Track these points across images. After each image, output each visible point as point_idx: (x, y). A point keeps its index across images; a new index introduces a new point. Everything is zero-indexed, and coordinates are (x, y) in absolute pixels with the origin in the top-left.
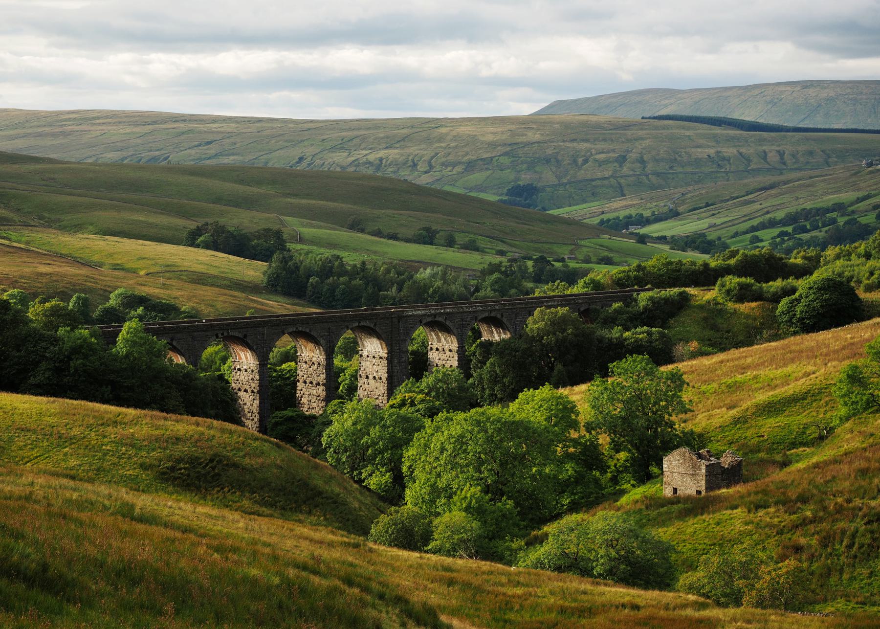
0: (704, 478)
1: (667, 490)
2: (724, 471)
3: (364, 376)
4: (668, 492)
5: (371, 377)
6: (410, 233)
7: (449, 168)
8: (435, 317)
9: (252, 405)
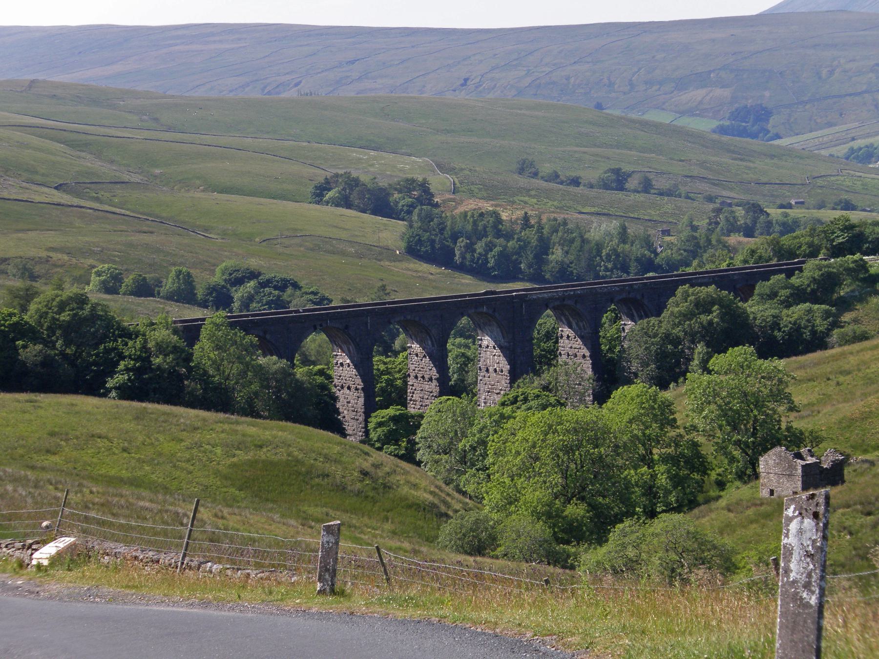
0: (800, 479)
1: (764, 491)
3: (484, 370)
4: (765, 493)
5: (491, 369)
7: (656, 87)
8: (564, 300)
9: (357, 404)
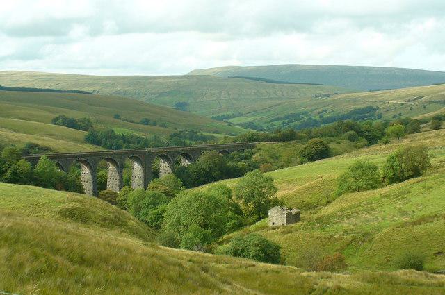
2: (293, 216)
6: (138, 120)
